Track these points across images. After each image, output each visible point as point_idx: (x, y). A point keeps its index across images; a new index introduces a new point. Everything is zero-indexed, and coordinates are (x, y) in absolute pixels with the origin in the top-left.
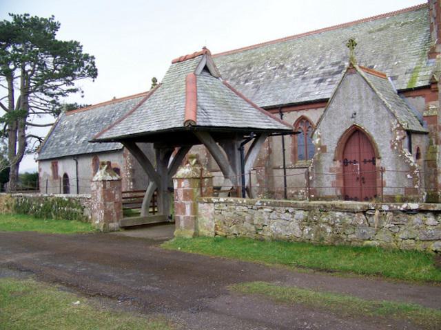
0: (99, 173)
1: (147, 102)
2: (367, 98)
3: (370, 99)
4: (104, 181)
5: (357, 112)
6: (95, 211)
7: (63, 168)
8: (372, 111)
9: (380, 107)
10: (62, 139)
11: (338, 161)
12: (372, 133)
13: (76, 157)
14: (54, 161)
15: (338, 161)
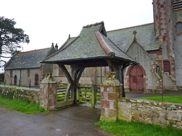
0: (45, 79)
1: (72, 44)
2: (141, 53)
3: (142, 53)
4: (49, 84)
5: (137, 58)
6: (42, 99)
7: (15, 73)
8: (143, 57)
9: (146, 56)
10: (15, 62)
11: (128, 76)
12: (143, 66)
13: (21, 69)
14: (11, 71)
15: (128, 76)
